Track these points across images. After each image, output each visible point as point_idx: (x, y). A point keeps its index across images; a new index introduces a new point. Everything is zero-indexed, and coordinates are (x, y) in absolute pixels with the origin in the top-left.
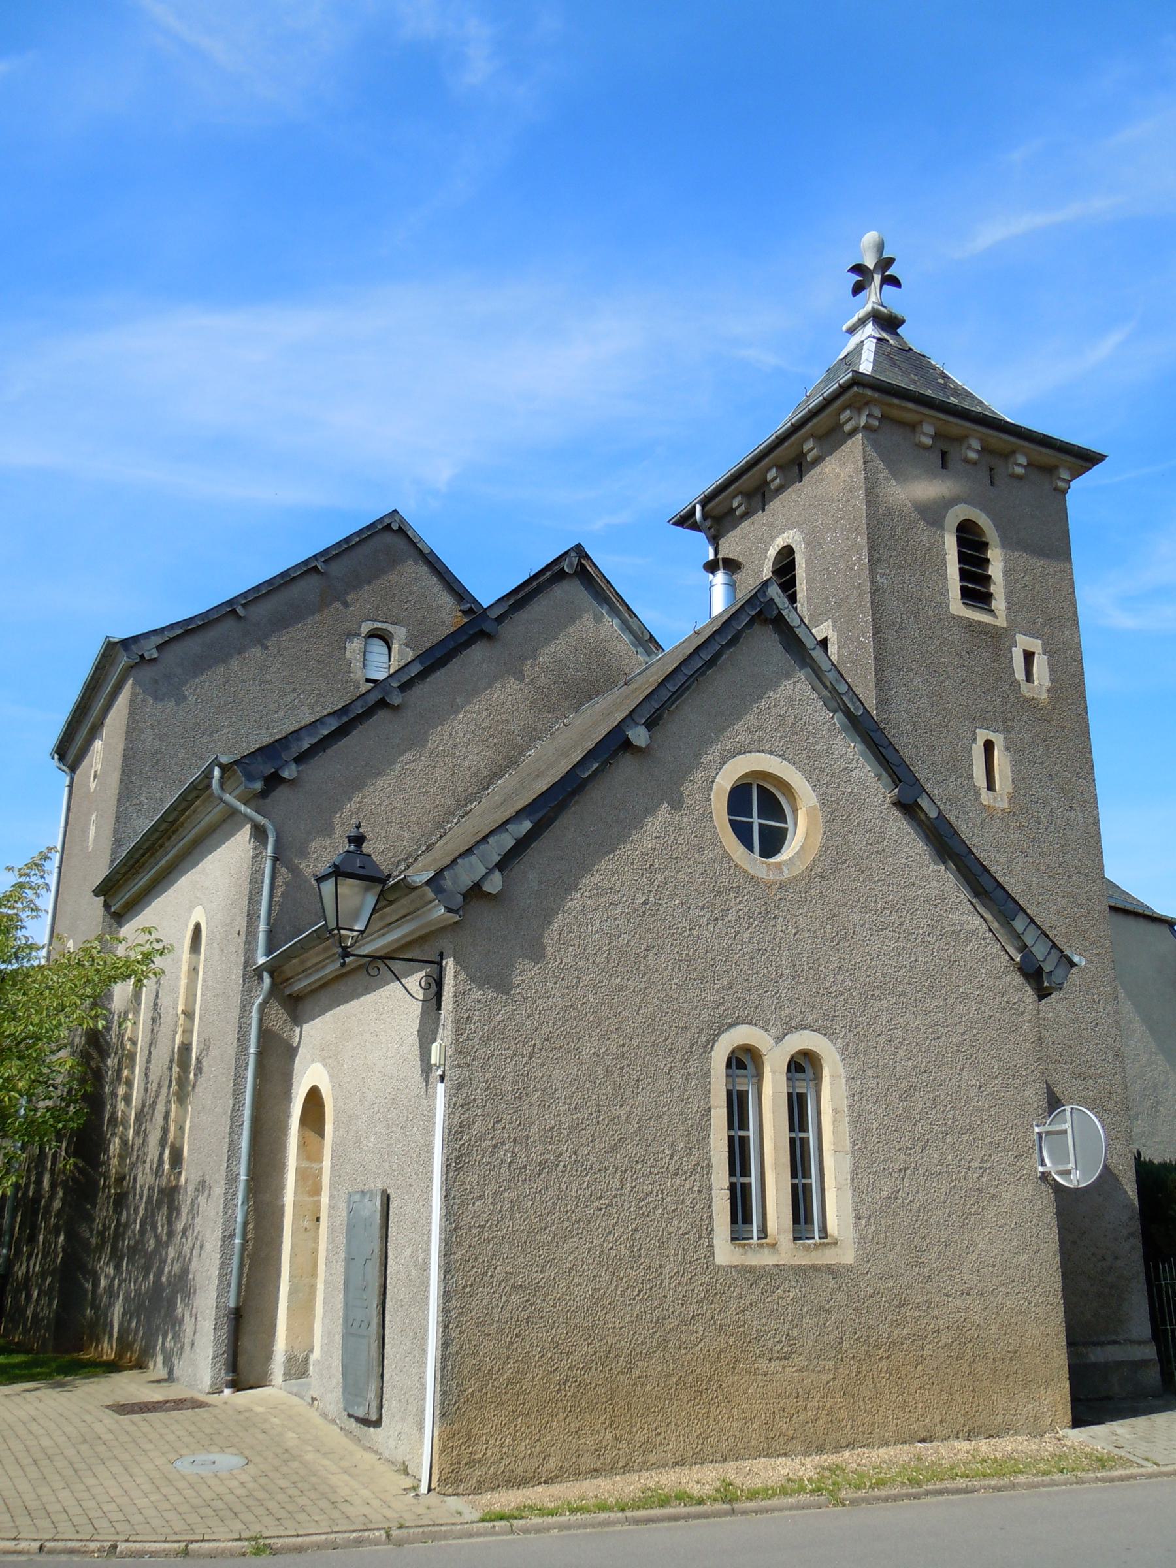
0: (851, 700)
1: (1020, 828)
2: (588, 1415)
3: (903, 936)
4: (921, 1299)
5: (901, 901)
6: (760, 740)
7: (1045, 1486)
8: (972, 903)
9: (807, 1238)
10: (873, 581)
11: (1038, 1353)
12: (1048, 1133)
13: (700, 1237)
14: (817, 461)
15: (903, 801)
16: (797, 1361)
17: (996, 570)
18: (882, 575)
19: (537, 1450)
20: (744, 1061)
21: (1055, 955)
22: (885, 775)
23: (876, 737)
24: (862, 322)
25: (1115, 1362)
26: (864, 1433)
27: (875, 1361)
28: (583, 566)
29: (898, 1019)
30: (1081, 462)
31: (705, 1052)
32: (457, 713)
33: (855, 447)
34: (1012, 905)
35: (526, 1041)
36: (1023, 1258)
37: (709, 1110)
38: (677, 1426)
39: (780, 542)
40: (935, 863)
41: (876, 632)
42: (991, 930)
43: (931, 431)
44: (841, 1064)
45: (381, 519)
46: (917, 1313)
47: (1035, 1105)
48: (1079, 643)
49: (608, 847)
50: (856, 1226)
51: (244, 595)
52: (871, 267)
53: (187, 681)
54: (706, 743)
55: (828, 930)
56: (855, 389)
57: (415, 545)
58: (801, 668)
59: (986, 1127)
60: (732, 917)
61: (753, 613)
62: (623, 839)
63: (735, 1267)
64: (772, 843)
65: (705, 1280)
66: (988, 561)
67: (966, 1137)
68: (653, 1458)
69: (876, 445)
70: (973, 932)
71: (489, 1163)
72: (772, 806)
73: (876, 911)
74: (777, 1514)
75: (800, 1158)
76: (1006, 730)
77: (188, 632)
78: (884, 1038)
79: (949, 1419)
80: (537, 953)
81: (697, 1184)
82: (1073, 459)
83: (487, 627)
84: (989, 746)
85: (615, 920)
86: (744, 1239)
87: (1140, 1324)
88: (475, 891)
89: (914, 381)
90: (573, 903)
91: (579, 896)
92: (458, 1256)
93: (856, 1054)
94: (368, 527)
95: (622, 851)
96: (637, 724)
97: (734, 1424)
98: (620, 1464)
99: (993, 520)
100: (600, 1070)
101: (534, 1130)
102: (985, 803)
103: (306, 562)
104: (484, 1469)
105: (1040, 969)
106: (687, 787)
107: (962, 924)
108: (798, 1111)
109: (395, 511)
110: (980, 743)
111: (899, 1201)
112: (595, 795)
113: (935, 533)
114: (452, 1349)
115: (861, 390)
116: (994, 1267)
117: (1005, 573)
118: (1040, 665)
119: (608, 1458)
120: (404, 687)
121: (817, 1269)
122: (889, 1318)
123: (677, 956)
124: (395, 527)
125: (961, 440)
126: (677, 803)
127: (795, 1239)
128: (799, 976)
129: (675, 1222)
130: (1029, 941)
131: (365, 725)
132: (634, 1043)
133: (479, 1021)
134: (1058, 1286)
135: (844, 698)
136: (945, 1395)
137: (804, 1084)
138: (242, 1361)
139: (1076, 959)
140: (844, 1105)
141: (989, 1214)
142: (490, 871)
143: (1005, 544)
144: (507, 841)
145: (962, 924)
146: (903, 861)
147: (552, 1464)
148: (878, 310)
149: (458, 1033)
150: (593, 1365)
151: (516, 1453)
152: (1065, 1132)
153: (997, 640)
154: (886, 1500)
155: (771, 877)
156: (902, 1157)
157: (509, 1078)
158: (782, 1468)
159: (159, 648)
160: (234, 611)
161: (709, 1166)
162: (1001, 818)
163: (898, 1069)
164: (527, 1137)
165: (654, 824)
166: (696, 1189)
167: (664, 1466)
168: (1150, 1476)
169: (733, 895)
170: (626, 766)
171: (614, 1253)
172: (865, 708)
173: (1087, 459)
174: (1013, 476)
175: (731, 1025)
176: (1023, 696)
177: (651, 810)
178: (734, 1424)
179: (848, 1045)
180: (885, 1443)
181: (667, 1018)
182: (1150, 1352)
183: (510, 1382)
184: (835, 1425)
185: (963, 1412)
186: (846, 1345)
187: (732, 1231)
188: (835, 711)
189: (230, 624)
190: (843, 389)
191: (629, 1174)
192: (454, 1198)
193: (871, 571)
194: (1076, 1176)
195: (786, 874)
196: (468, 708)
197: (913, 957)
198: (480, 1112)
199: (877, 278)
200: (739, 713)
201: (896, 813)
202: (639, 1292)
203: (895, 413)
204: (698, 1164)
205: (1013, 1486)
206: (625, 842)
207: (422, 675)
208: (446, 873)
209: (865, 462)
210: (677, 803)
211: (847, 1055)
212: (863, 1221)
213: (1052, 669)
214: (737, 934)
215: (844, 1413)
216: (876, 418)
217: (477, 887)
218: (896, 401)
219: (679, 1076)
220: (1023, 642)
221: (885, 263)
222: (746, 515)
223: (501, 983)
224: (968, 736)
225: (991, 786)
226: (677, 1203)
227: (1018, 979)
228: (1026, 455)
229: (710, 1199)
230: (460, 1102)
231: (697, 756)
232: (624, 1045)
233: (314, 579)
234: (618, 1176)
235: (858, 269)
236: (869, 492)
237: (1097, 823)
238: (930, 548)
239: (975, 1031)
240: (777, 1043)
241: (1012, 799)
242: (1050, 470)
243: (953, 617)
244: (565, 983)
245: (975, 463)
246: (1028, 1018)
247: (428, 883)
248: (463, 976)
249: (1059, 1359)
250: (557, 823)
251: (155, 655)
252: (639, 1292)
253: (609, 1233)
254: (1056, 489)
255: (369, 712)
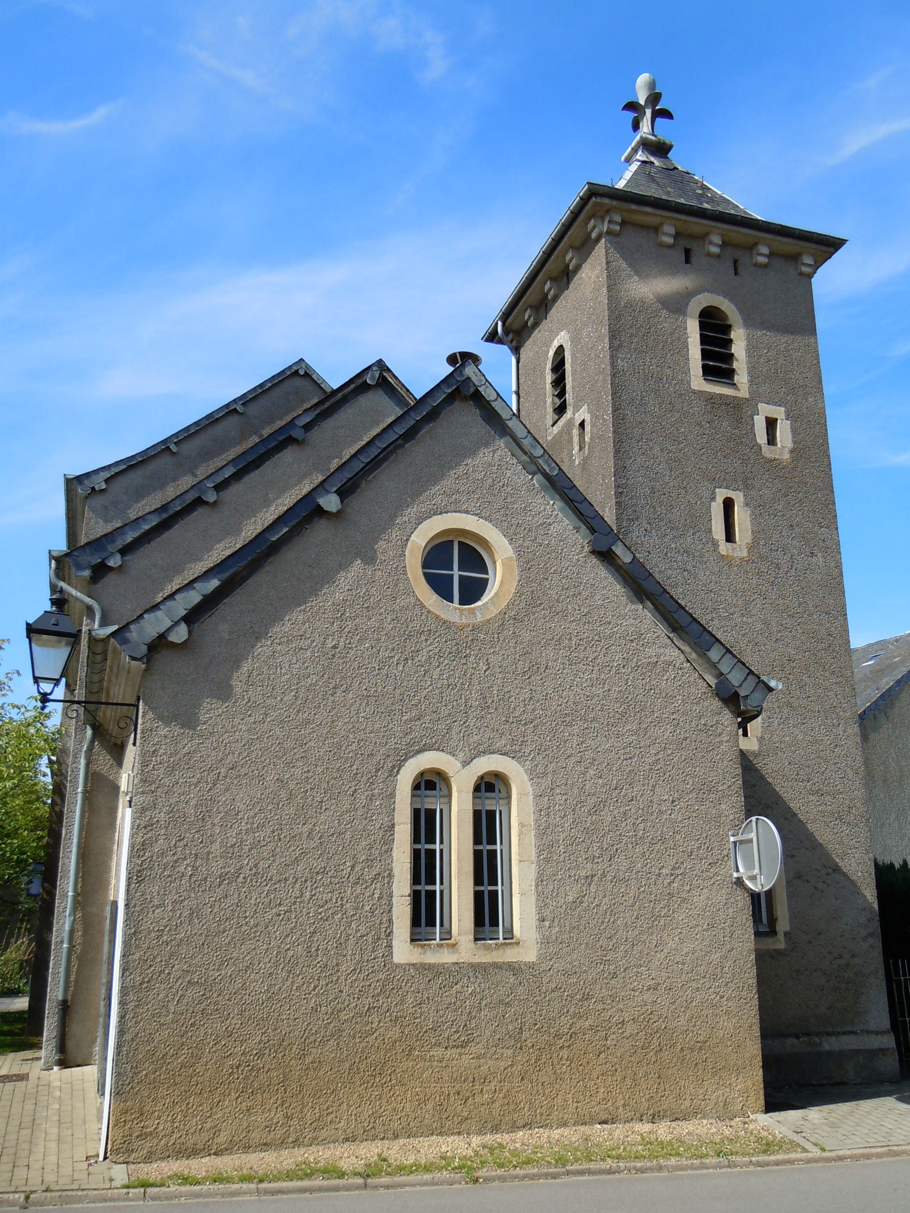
0: (547, 462)
1: (759, 574)
2: (259, 1096)
3: (596, 668)
4: (605, 993)
5: (597, 638)
6: (457, 502)
7: (695, 1169)
8: (669, 637)
9: (491, 939)
10: (613, 364)
11: (729, 1043)
12: (741, 842)
13: (378, 939)
14: (578, 268)
15: (598, 549)
16: (473, 1049)
17: (739, 348)
18: (623, 359)
19: (208, 1125)
20: (430, 782)
21: (752, 681)
22: (583, 527)
23: (571, 494)
24: (635, 151)
25: (850, 1051)
26: (541, 1115)
27: (564, 1048)
28: (385, 379)
29: (589, 742)
30: (823, 248)
31: (390, 775)
32: (269, 506)
33: (600, 251)
34: (707, 637)
35: (211, 770)
36: (715, 957)
37: (393, 826)
38: (349, 1106)
39: (556, 344)
40: (632, 602)
41: (615, 409)
42: (688, 661)
43: (672, 231)
44: (529, 784)
45: (290, 367)
46: (600, 1007)
47: (731, 817)
48: (823, 408)
49: (298, 598)
50: (540, 927)
51: (176, 435)
52: (642, 102)
53: (131, 506)
54: (400, 506)
55: (520, 666)
56: (594, 199)
57: (319, 385)
58: (501, 437)
59: (678, 837)
60: (422, 657)
61: (449, 391)
62: (314, 592)
63: (414, 965)
64: (472, 591)
65: (381, 976)
66: (731, 341)
67: (657, 847)
68: (323, 1134)
69: (619, 248)
70: (670, 663)
71: (169, 876)
72: (473, 556)
73: (570, 647)
74: (407, 1189)
75: (486, 868)
76: (746, 487)
77: (130, 467)
78: (573, 759)
79: (633, 1103)
80: (224, 692)
81: (378, 891)
82: (813, 246)
83: (297, 433)
84: (728, 505)
85: (304, 663)
86: (426, 940)
87: (878, 1014)
88: (160, 644)
89: (669, 193)
90: (263, 649)
91: (269, 643)
92: (137, 956)
93: (545, 774)
94: (279, 374)
95: (314, 603)
96: (328, 492)
97: (408, 1105)
98: (291, 1139)
99: (736, 305)
100: (283, 794)
101: (216, 847)
102: (724, 553)
103: (227, 406)
104: (155, 1141)
105: (736, 694)
106: (381, 545)
107: (658, 656)
108: (486, 826)
109: (302, 360)
110: (720, 500)
111: (585, 905)
112: (289, 555)
113: (677, 319)
114: (127, 1037)
115: (599, 200)
116: (684, 964)
117: (748, 351)
118: (783, 431)
119: (279, 1133)
120: (219, 488)
121: (497, 966)
122: (572, 1010)
123: (365, 693)
124: (302, 372)
125: (703, 237)
126: (370, 559)
127: (476, 939)
128: (488, 707)
129: (354, 925)
130: (724, 668)
131: (186, 520)
132: (319, 769)
133: (165, 754)
134: (753, 981)
135: (540, 461)
136: (628, 1081)
137: (494, 802)
138: (70, 1044)
139: (773, 684)
140: (531, 819)
141: (680, 917)
142: (176, 623)
143: (749, 323)
144: (194, 597)
145: (658, 656)
146: (600, 602)
147: (222, 1138)
148: (646, 139)
149: (144, 764)
150: (267, 1051)
151: (187, 1127)
152: (751, 841)
153: (738, 411)
154: (524, 1178)
155: (464, 621)
156: (589, 865)
157: (193, 803)
158: (430, 1148)
159: (107, 481)
160: (168, 448)
161: (390, 876)
162: (739, 566)
163: (587, 787)
164: (208, 853)
165: (346, 579)
166: (376, 896)
167: (334, 1142)
168: (816, 1160)
169: (423, 638)
170: (320, 531)
171: (291, 953)
172: (560, 469)
173: (829, 246)
174: (757, 265)
175: (419, 752)
176: (764, 457)
177: (343, 566)
178: (408, 1105)
179: (536, 766)
180: (564, 1124)
181: (354, 747)
182: (889, 1041)
183: (183, 1066)
184: (512, 1107)
185: (647, 1096)
186: (526, 1034)
187: (412, 934)
188: (534, 474)
189: (166, 459)
190: (584, 201)
191: (309, 883)
192: (135, 906)
193: (612, 357)
194: (761, 879)
195: (479, 618)
196: (279, 501)
197: (607, 687)
198: (163, 832)
199: (649, 112)
200: (435, 479)
201: (594, 560)
202: (315, 988)
203: (637, 218)
204: (379, 874)
205: (660, 1168)
206: (316, 595)
207: (238, 476)
208: (132, 627)
209: (607, 263)
210: (370, 559)
211: (534, 775)
212: (547, 923)
213: (795, 432)
214: (426, 672)
215: (521, 1096)
216: (616, 223)
217: (162, 637)
218: (633, 207)
219: (363, 797)
220: (766, 409)
221: (654, 98)
222: (536, 325)
223: (189, 721)
224: (707, 494)
225: (730, 537)
226: (357, 908)
227: (717, 704)
228: (768, 245)
229: (390, 905)
230: (143, 824)
231: (393, 517)
232: (308, 771)
233: (234, 420)
234: (298, 885)
235: (632, 106)
236: (610, 288)
237: (839, 565)
238: (672, 333)
239: (669, 752)
240: (464, 766)
241: (751, 548)
242: (794, 258)
243: (694, 392)
244: (252, 719)
245: (718, 256)
246: (726, 739)
247: (113, 634)
248: (150, 715)
249: (753, 1049)
250: (250, 581)
251: (104, 486)
252: (315, 988)
253: (287, 936)
254: (801, 274)
255: (188, 509)
